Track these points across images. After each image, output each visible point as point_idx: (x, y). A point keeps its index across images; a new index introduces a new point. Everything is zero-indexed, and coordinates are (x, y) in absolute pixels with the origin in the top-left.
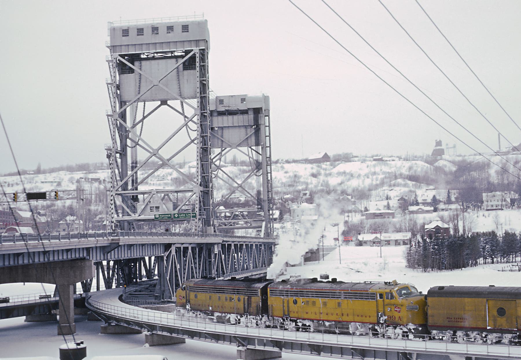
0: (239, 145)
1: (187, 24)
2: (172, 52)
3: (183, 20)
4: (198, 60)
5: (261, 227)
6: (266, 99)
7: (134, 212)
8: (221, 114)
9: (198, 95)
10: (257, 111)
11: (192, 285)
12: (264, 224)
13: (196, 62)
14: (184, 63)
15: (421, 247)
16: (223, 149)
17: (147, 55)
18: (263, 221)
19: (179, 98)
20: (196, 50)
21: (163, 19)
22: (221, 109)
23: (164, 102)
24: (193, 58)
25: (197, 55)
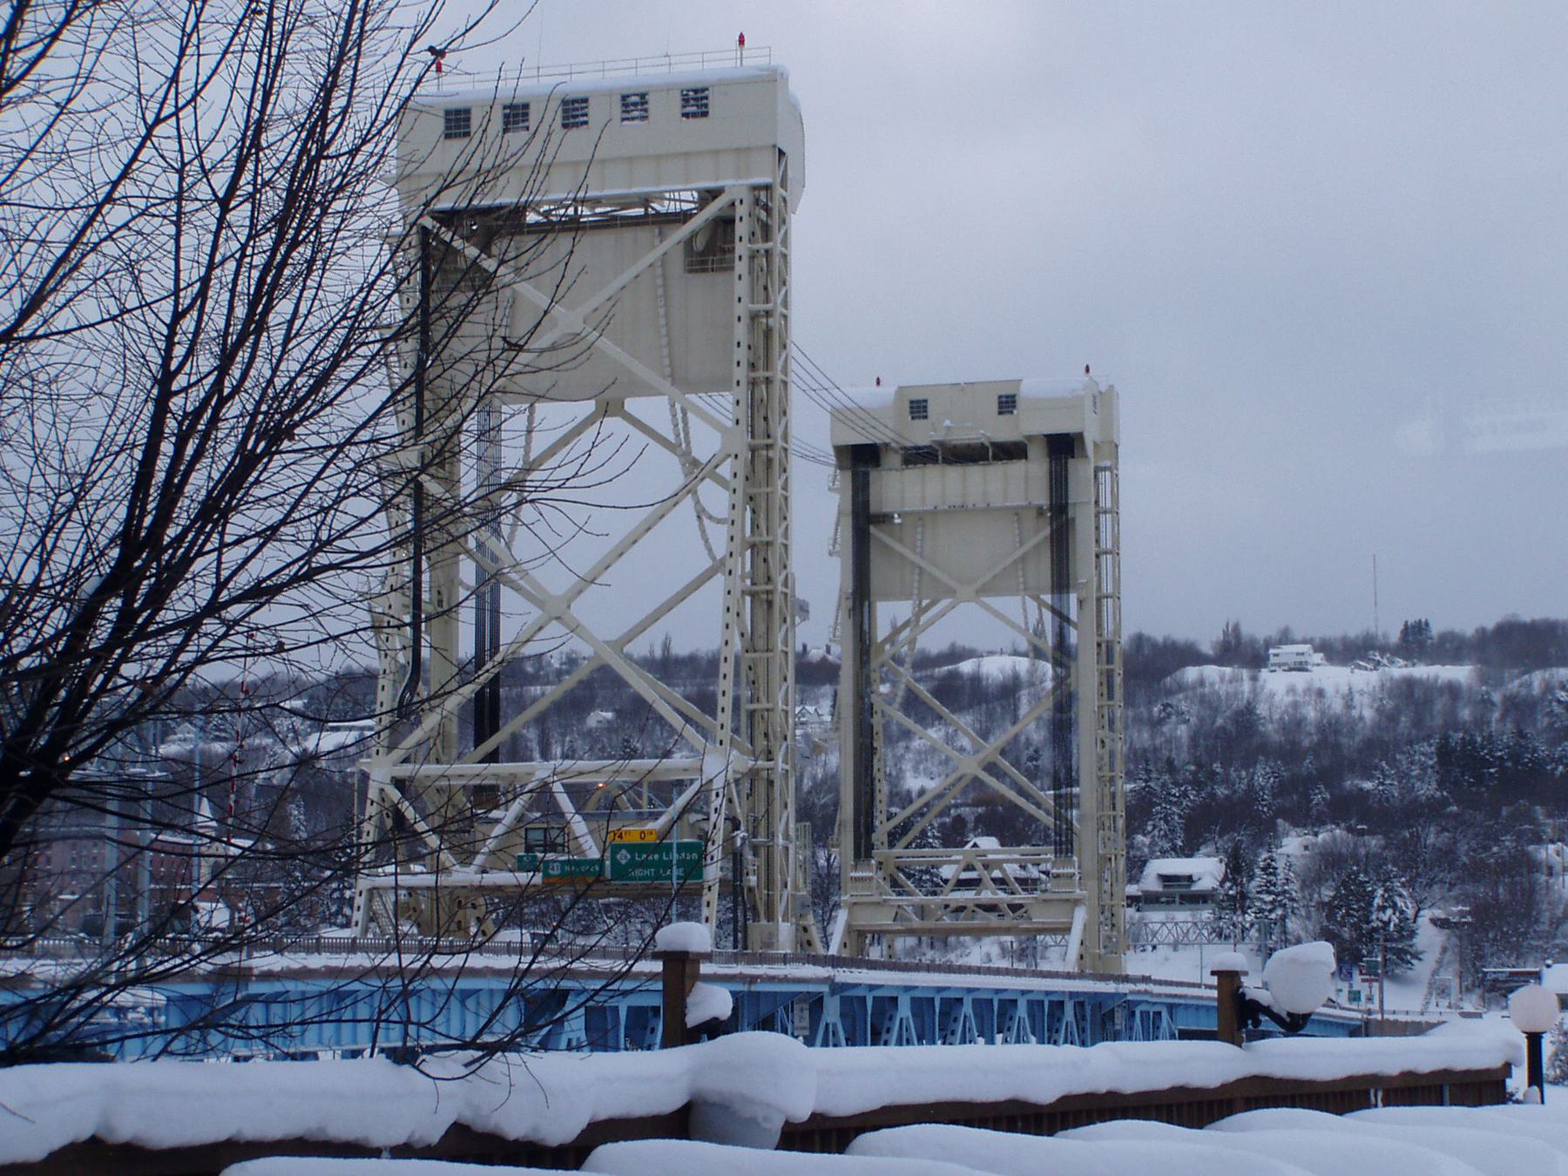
0: (987, 589)
1: (461, 106)
2: (645, 201)
3: (690, 70)
4: (741, 229)
5: (1066, 930)
6: (1104, 400)
7: (466, 856)
8: (919, 456)
9: (741, 373)
10: (1063, 447)
11: (146, 928)
12: (1080, 916)
13: (733, 242)
14: (689, 242)
15: (949, 815)
16: (925, 603)
17: (547, 214)
18: (1076, 902)
19: (666, 385)
20: (736, 186)
21: (706, 57)
22: (921, 434)
23: (610, 407)
24: (724, 224)
25: (741, 211)
